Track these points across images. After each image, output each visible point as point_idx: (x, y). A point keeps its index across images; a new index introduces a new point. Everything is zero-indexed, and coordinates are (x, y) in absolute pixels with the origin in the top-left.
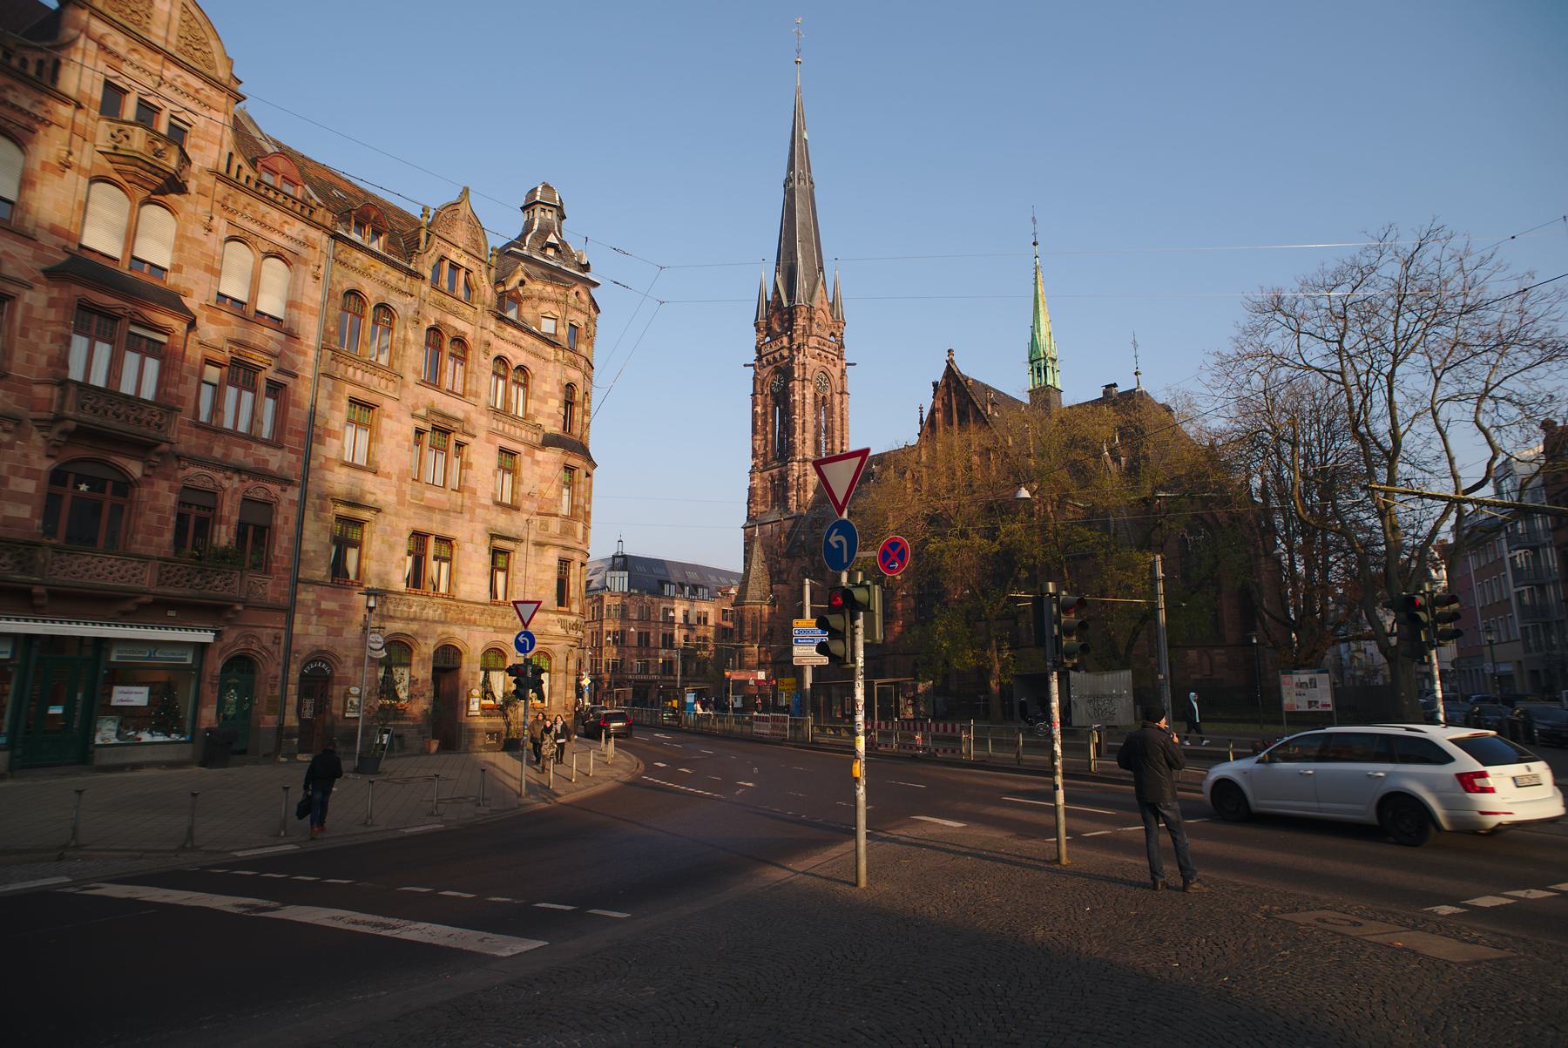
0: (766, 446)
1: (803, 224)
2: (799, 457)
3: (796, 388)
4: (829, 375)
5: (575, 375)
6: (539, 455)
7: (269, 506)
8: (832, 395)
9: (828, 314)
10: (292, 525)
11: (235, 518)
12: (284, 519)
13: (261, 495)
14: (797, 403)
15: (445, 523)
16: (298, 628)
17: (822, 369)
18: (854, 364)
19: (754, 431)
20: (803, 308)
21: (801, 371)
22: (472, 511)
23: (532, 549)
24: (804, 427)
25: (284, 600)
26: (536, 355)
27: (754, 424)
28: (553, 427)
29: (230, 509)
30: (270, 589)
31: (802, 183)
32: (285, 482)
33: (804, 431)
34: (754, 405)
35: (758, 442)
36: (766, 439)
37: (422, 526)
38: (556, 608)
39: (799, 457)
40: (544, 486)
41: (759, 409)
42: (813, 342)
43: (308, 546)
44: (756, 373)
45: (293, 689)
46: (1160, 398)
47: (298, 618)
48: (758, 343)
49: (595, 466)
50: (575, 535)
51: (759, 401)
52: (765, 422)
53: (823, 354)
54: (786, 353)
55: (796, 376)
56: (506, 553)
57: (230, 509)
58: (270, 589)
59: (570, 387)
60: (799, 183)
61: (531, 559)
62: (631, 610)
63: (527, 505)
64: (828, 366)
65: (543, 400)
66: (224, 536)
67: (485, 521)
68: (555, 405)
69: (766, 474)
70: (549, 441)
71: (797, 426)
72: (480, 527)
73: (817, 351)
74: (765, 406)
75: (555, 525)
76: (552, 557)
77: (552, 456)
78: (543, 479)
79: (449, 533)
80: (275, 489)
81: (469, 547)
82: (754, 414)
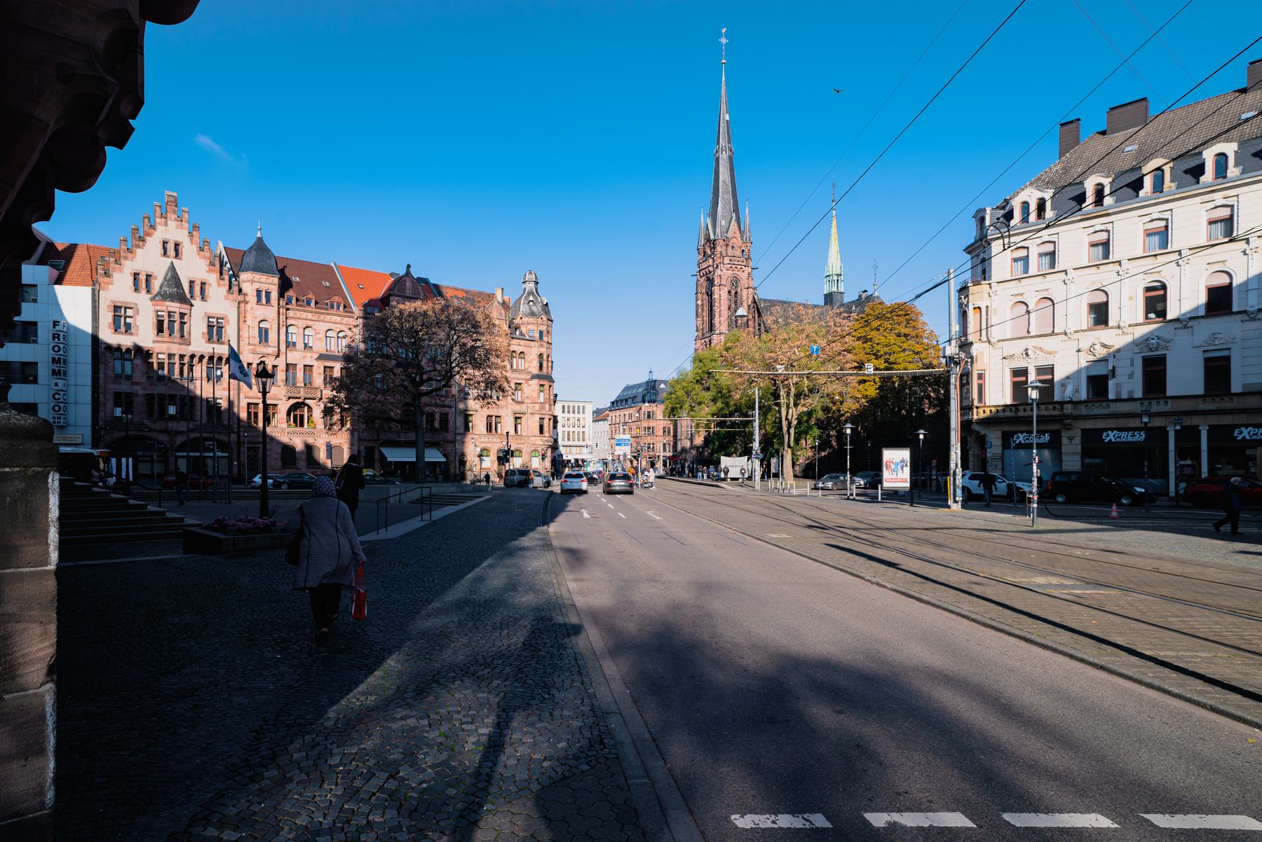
0: (703, 324)
1: (724, 182)
2: (717, 332)
3: (716, 291)
4: (739, 278)
5: (543, 350)
6: (530, 382)
7: (447, 414)
8: (741, 290)
9: (739, 239)
10: (453, 419)
11: (439, 419)
12: (451, 418)
13: (444, 412)
14: (716, 300)
15: (498, 411)
16: (457, 447)
17: (733, 276)
18: (757, 268)
19: (697, 316)
20: (720, 240)
21: (719, 280)
22: (507, 406)
23: (530, 416)
24: (720, 314)
25: (453, 440)
26: (527, 346)
27: (697, 311)
28: (535, 371)
29: (437, 417)
30: (449, 437)
31: (724, 153)
32: (450, 407)
33: (720, 316)
34: (697, 300)
35: (699, 322)
36: (703, 320)
37: (490, 414)
38: (539, 435)
39: (717, 332)
40: (532, 393)
41: (699, 302)
42: (727, 260)
43: (458, 424)
44: (698, 280)
45: (457, 463)
46: (675, 376)
47: (457, 444)
48: (699, 261)
49: (553, 382)
50: (545, 409)
51: (700, 297)
52: (703, 310)
53: (734, 266)
54: (711, 269)
55: (716, 283)
56: (520, 418)
57: (437, 417)
58: (449, 437)
59: (541, 355)
60: (722, 153)
61: (529, 419)
62: (658, 414)
63: (526, 401)
64: (739, 273)
65: (530, 362)
66: (437, 424)
67: (512, 409)
68: (536, 364)
69: (703, 341)
70: (534, 377)
71: (716, 313)
72: (509, 411)
73: (730, 266)
74: (702, 301)
75: (537, 407)
76: (537, 418)
77: (535, 382)
78: (533, 391)
79: (499, 415)
80: (447, 409)
81: (506, 418)
82: (697, 305)
